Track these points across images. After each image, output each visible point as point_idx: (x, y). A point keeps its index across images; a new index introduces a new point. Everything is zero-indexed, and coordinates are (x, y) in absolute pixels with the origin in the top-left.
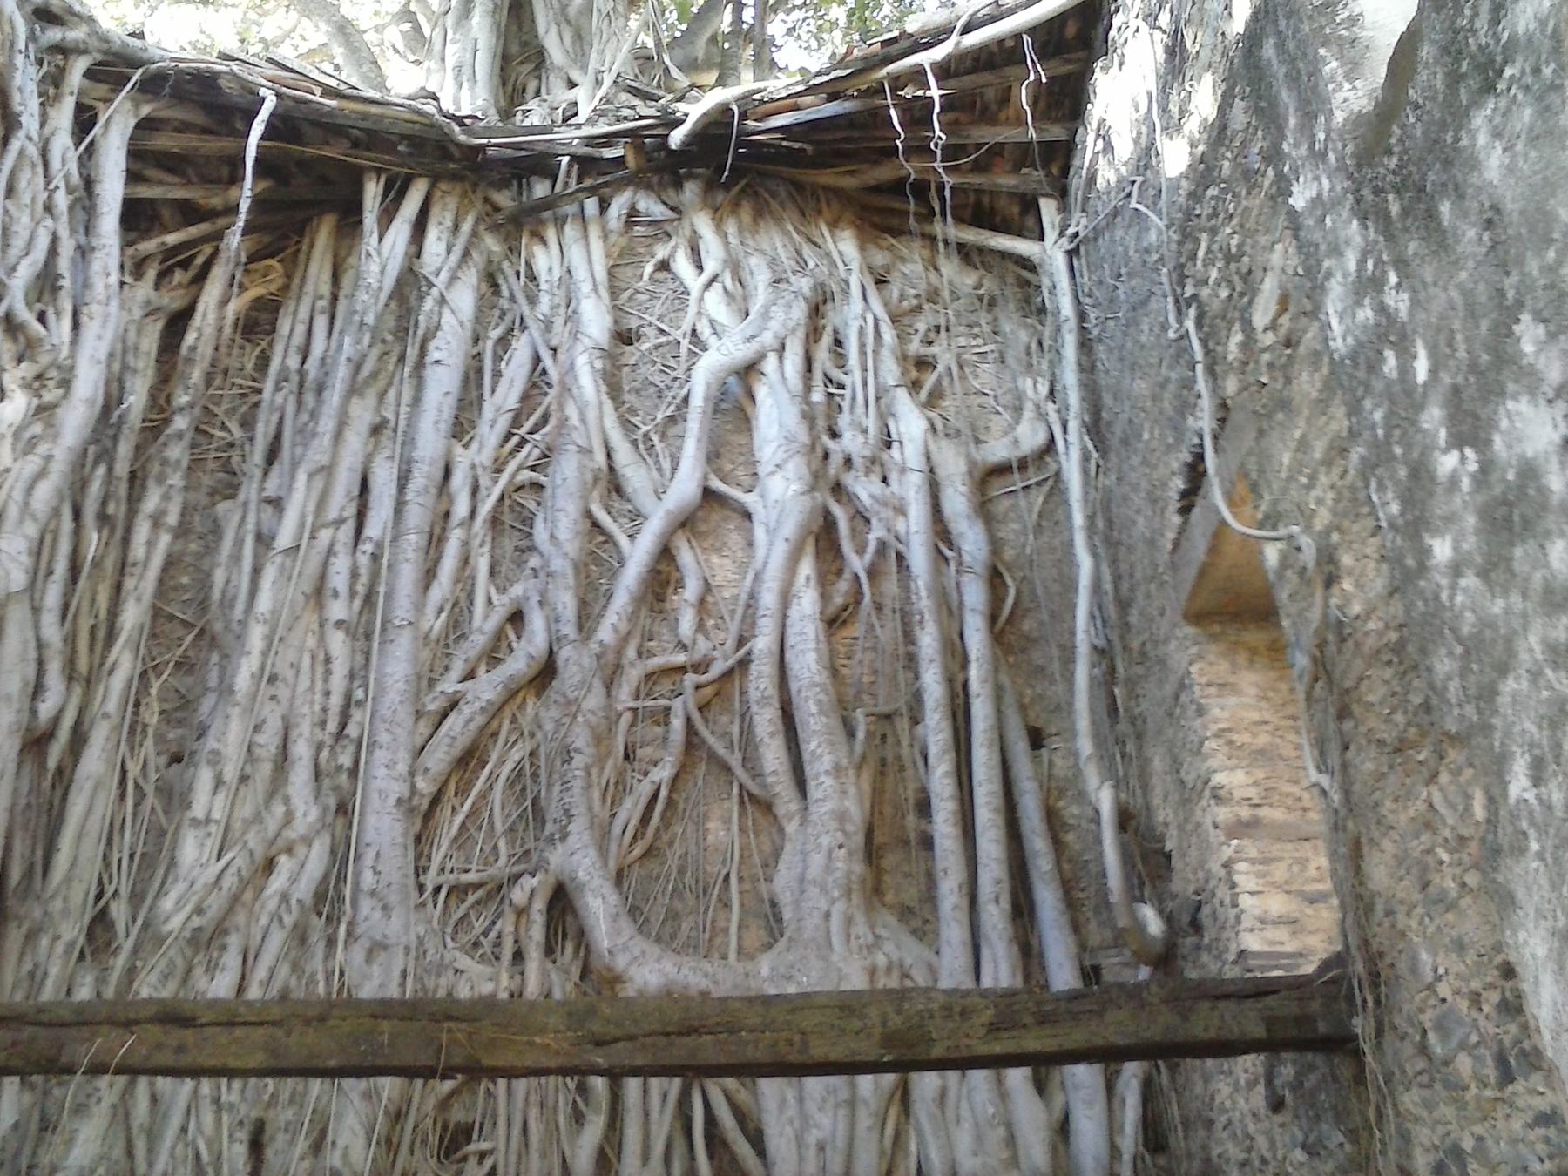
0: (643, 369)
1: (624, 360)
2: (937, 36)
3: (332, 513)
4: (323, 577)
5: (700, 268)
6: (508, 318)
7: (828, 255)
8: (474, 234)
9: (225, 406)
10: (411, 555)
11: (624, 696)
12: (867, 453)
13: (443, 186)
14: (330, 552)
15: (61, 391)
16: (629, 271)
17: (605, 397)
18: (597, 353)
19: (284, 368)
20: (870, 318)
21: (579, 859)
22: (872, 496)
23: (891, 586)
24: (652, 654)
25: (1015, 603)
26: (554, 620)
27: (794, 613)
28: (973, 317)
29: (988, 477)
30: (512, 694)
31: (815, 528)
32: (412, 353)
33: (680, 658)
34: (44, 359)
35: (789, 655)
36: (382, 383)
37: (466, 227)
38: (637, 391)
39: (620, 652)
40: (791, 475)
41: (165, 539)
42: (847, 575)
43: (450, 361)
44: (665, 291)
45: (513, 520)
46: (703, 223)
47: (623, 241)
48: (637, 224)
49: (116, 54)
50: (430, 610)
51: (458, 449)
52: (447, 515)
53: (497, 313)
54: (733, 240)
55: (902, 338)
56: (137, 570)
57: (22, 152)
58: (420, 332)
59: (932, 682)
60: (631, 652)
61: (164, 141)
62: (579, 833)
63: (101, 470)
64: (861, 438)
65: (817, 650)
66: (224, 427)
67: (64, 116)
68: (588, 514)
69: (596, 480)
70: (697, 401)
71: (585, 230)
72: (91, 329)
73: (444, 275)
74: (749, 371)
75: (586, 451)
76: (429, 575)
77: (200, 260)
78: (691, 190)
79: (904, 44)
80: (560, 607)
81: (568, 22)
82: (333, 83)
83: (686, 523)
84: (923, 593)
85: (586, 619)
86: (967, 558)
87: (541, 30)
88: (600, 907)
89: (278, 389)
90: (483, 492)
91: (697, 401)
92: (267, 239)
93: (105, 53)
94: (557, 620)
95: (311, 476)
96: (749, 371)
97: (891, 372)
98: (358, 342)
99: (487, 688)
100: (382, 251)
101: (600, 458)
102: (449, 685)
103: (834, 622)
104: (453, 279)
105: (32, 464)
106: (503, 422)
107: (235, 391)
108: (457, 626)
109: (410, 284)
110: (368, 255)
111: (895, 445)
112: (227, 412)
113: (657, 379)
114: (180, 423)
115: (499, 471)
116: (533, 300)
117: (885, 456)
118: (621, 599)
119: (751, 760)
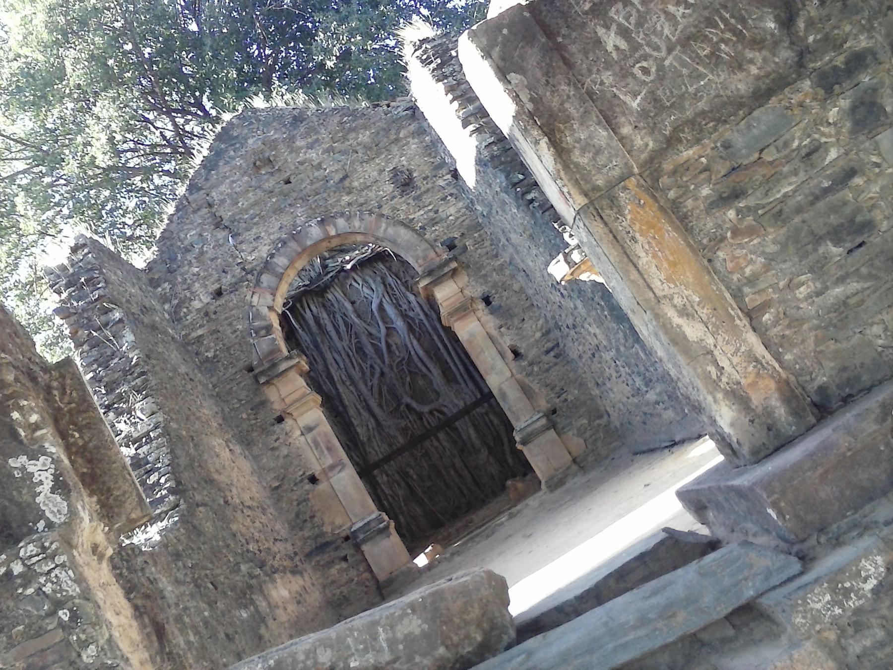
11: (395, 369)
21: (407, 399)
23: (424, 328)
26: (379, 366)
30: (379, 380)
45: (360, 349)
59: (439, 345)
62: (405, 396)
76: (354, 368)
88: (414, 404)
99: (375, 382)
102: (370, 384)
103: (418, 340)
108: (363, 373)
118: (386, 355)
119: (420, 371)
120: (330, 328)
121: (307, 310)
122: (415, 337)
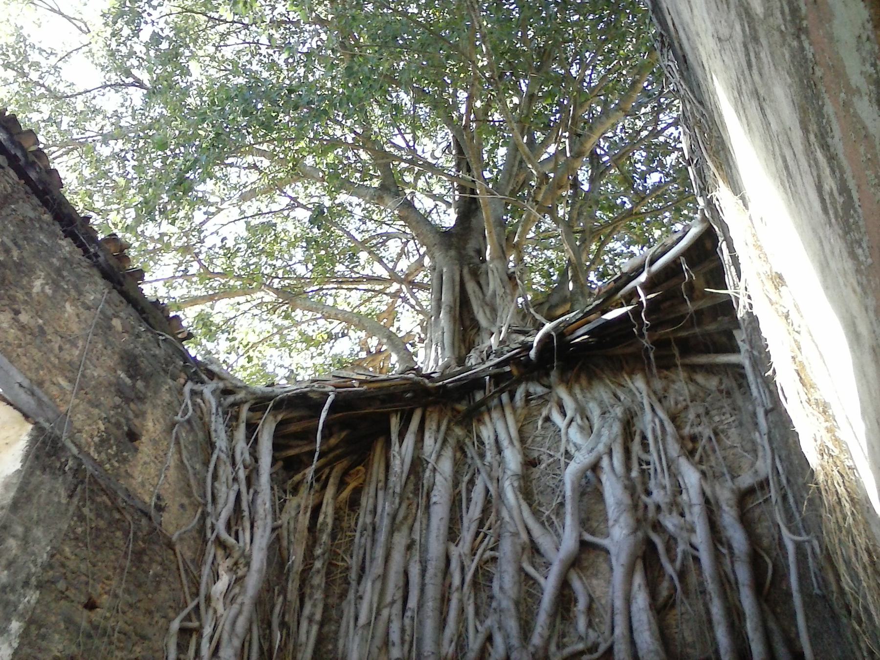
0: (543, 479)
1: (533, 477)
2: (638, 271)
3: (388, 599)
4: (387, 634)
5: (564, 415)
6: (472, 468)
7: (631, 390)
8: (448, 428)
9: (343, 548)
10: (430, 614)
12: (667, 500)
13: (430, 409)
14: (389, 621)
15: (246, 569)
16: (531, 426)
17: (522, 502)
18: (515, 478)
19: (365, 524)
20: (657, 421)
22: (674, 525)
23: (693, 579)
24: (564, 646)
25: (773, 574)
26: (507, 637)
27: (634, 608)
28: (720, 404)
29: (744, 497)
31: (640, 553)
32: (423, 502)
33: (581, 646)
34: (236, 555)
35: (635, 635)
36: (410, 521)
37: (443, 428)
38: (542, 492)
39: (546, 648)
40: (622, 524)
41: (315, 628)
42: (667, 577)
43: (441, 501)
44: (550, 433)
45: (482, 580)
46: (562, 392)
47: (525, 411)
48: (532, 400)
49: (261, 398)
50: (446, 642)
51: (452, 547)
52: (450, 586)
53: (467, 466)
54: (579, 396)
55: (678, 428)
56: (303, 648)
57: (218, 458)
58: (425, 489)
60: (553, 648)
61: (293, 428)
63: (281, 599)
64: (662, 493)
65: (650, 629)
66: (343, 560)
67: (241, 433)
68: (521, 569)
69: (523, 549)
70: (568, 493)
71: (503, 410)
72: (258, 532)
73: (434, 456)
74: (595, 467)
75: (516, 534)
77: (324, 477)
78: (554, 375)
79: (624, 279)
80: (509, 630)
81: (487, 304)
82: (363, 377)
83: (575, 563)
84: (709, 581)
85: (526, 630)
86: (736, 551)
87: (476, 312)
89: (362, 535)
90: (466, 569)
91: (568, 493)
92: (355, 457)
93: (254, 399)
94: (508, 637)
95: (373, 582)
96: (595, 467)
97: (674, 449)
98: (393, 503)
100: (402, 452)
101: (524, 536)
104: (439, 456)
105: (235, 607)
106: (474, 527)
107: (347, 539)
109: (417, 465)
110: (394, 456)
111: (684, 491)
112: (344, 552)
113: (551, 483)
114: (318, 564)
115: (475, 555)
116: (482, 456)
117: (679, 499)
120: (441, 496)
121: (410, 439)
122: (653, 594)
